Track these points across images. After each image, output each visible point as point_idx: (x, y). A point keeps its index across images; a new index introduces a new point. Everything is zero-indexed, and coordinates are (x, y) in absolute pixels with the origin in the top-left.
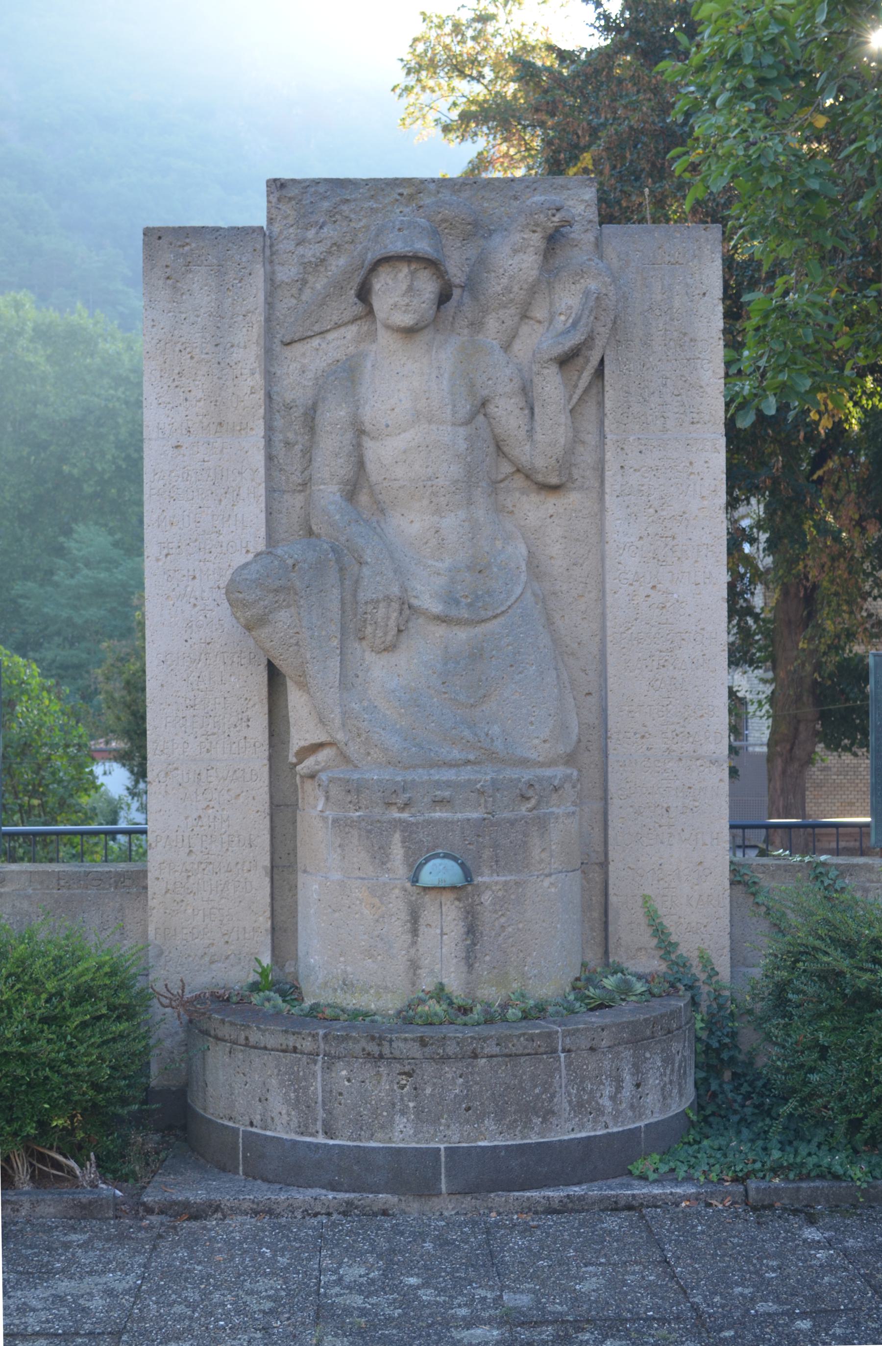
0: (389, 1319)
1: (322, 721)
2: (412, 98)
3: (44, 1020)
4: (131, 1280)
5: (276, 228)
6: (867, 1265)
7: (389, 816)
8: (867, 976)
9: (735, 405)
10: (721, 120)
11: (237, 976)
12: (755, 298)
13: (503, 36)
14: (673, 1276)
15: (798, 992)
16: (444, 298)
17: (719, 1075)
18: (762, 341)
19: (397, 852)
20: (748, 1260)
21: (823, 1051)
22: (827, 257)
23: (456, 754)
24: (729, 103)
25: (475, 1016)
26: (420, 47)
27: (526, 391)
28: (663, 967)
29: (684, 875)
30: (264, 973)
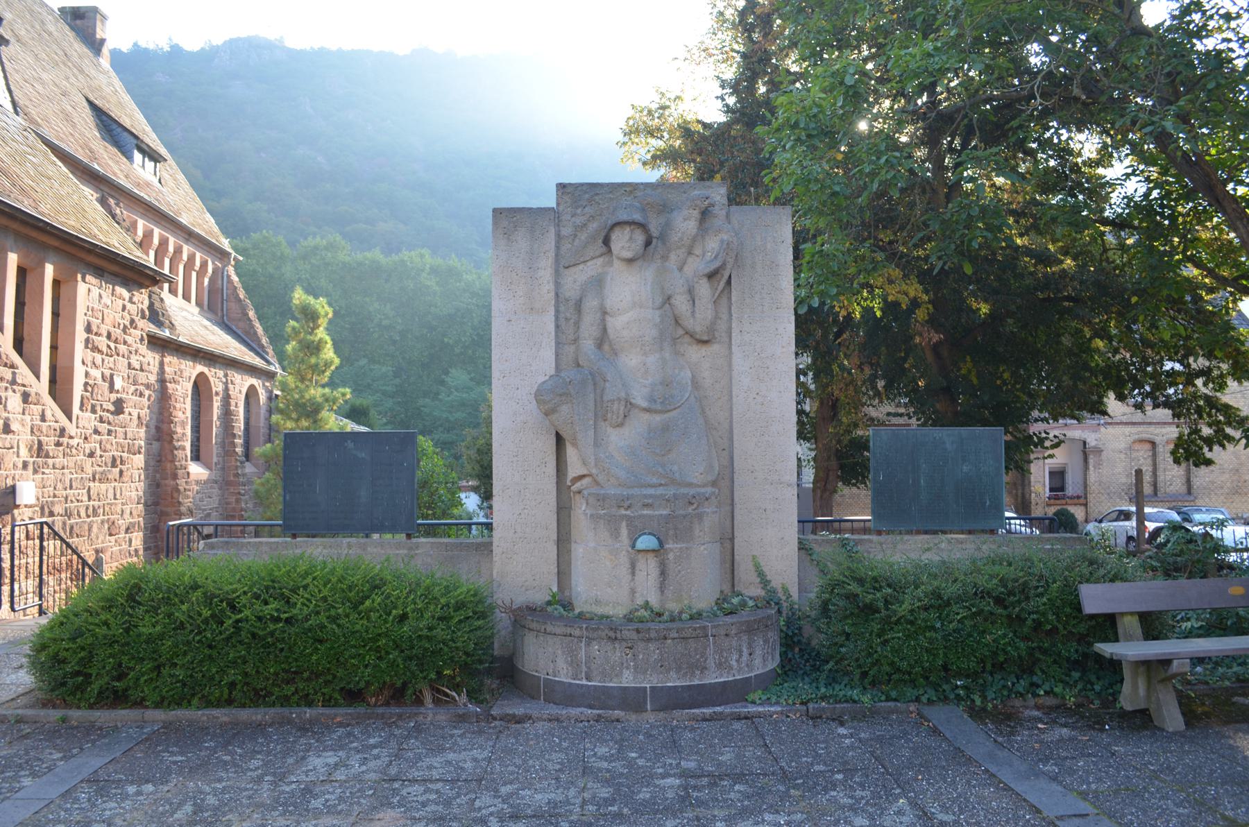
0: (622, 774)
1: (584, 463)
2: (627, 148)
3: (440, 619)
4: (486, 754)
5: (561, 208)
6: (871, 746)
7: (621, 513)
8: (870, 596)
9: (799, 302)
10: (789, 155)
11: (539, 597)
12: (807, 246)
13: (675, 115)
14: (770, 753)
15: (834, 605)
16: (648, 243)
17: (792, 650)
18: (811, 269)
19: (624, 532)
20: (810, 744)
21: (848, 635)
22: (845, 226)
23: (655, 480)
24: (792, 147)
25: (665, 617)
26: (631, 122)
27: (691, 291)
28: (763, 593)
29: (774, 545)
30: (554, 596)
